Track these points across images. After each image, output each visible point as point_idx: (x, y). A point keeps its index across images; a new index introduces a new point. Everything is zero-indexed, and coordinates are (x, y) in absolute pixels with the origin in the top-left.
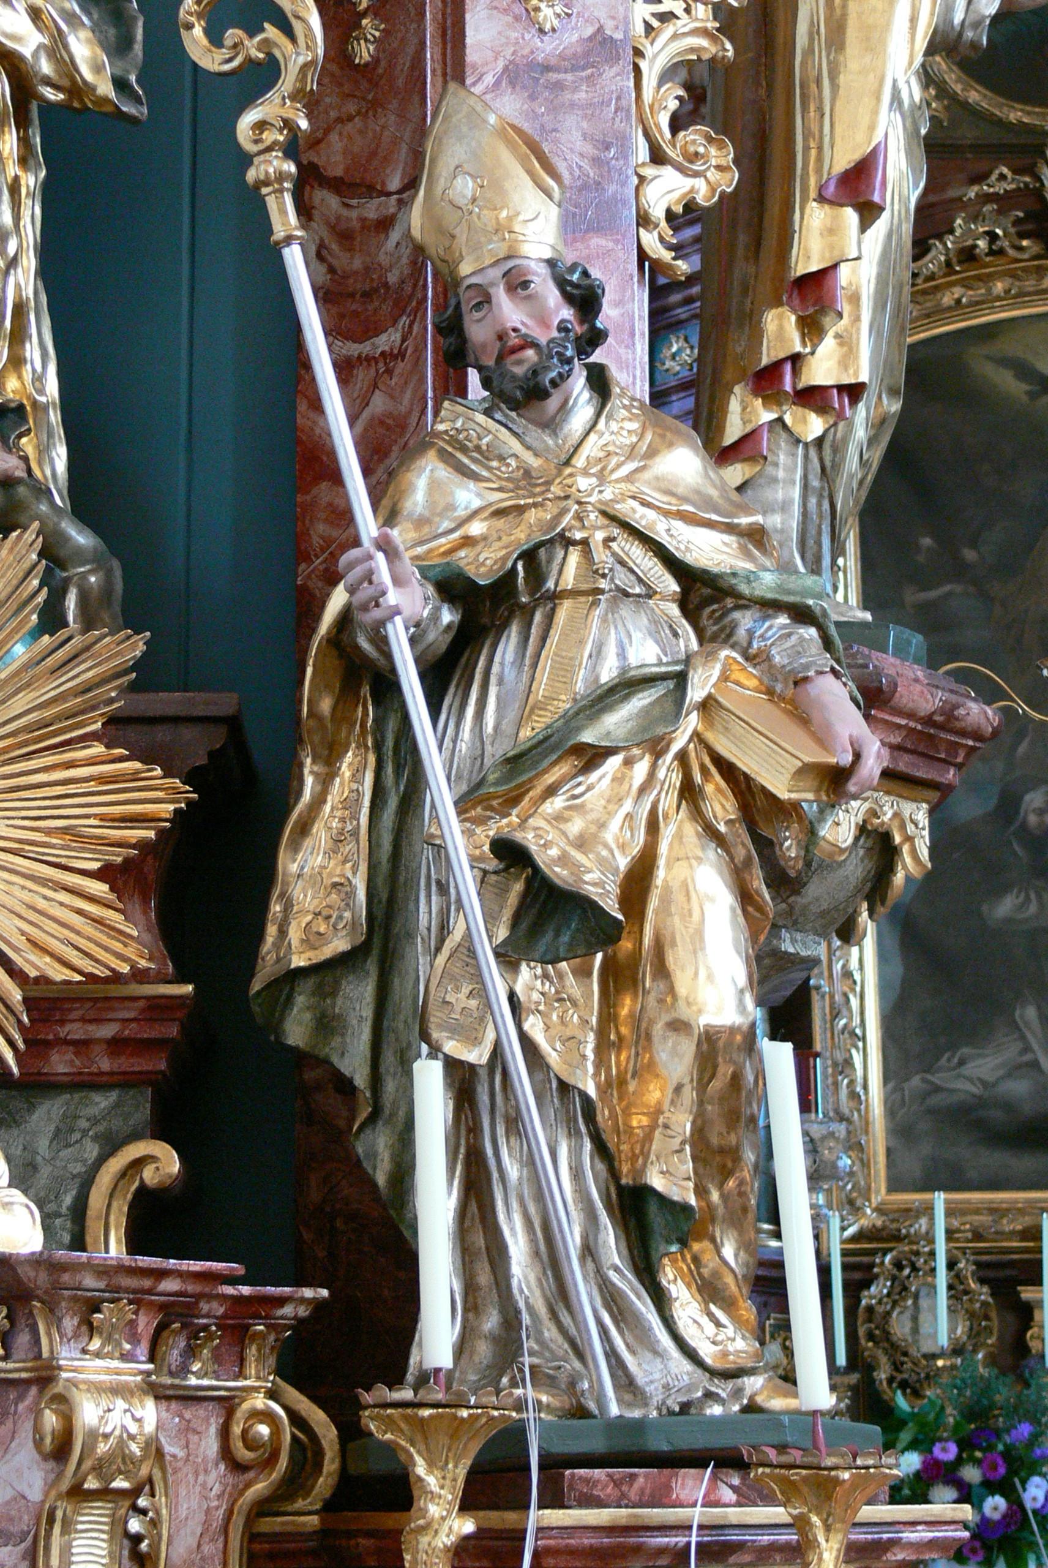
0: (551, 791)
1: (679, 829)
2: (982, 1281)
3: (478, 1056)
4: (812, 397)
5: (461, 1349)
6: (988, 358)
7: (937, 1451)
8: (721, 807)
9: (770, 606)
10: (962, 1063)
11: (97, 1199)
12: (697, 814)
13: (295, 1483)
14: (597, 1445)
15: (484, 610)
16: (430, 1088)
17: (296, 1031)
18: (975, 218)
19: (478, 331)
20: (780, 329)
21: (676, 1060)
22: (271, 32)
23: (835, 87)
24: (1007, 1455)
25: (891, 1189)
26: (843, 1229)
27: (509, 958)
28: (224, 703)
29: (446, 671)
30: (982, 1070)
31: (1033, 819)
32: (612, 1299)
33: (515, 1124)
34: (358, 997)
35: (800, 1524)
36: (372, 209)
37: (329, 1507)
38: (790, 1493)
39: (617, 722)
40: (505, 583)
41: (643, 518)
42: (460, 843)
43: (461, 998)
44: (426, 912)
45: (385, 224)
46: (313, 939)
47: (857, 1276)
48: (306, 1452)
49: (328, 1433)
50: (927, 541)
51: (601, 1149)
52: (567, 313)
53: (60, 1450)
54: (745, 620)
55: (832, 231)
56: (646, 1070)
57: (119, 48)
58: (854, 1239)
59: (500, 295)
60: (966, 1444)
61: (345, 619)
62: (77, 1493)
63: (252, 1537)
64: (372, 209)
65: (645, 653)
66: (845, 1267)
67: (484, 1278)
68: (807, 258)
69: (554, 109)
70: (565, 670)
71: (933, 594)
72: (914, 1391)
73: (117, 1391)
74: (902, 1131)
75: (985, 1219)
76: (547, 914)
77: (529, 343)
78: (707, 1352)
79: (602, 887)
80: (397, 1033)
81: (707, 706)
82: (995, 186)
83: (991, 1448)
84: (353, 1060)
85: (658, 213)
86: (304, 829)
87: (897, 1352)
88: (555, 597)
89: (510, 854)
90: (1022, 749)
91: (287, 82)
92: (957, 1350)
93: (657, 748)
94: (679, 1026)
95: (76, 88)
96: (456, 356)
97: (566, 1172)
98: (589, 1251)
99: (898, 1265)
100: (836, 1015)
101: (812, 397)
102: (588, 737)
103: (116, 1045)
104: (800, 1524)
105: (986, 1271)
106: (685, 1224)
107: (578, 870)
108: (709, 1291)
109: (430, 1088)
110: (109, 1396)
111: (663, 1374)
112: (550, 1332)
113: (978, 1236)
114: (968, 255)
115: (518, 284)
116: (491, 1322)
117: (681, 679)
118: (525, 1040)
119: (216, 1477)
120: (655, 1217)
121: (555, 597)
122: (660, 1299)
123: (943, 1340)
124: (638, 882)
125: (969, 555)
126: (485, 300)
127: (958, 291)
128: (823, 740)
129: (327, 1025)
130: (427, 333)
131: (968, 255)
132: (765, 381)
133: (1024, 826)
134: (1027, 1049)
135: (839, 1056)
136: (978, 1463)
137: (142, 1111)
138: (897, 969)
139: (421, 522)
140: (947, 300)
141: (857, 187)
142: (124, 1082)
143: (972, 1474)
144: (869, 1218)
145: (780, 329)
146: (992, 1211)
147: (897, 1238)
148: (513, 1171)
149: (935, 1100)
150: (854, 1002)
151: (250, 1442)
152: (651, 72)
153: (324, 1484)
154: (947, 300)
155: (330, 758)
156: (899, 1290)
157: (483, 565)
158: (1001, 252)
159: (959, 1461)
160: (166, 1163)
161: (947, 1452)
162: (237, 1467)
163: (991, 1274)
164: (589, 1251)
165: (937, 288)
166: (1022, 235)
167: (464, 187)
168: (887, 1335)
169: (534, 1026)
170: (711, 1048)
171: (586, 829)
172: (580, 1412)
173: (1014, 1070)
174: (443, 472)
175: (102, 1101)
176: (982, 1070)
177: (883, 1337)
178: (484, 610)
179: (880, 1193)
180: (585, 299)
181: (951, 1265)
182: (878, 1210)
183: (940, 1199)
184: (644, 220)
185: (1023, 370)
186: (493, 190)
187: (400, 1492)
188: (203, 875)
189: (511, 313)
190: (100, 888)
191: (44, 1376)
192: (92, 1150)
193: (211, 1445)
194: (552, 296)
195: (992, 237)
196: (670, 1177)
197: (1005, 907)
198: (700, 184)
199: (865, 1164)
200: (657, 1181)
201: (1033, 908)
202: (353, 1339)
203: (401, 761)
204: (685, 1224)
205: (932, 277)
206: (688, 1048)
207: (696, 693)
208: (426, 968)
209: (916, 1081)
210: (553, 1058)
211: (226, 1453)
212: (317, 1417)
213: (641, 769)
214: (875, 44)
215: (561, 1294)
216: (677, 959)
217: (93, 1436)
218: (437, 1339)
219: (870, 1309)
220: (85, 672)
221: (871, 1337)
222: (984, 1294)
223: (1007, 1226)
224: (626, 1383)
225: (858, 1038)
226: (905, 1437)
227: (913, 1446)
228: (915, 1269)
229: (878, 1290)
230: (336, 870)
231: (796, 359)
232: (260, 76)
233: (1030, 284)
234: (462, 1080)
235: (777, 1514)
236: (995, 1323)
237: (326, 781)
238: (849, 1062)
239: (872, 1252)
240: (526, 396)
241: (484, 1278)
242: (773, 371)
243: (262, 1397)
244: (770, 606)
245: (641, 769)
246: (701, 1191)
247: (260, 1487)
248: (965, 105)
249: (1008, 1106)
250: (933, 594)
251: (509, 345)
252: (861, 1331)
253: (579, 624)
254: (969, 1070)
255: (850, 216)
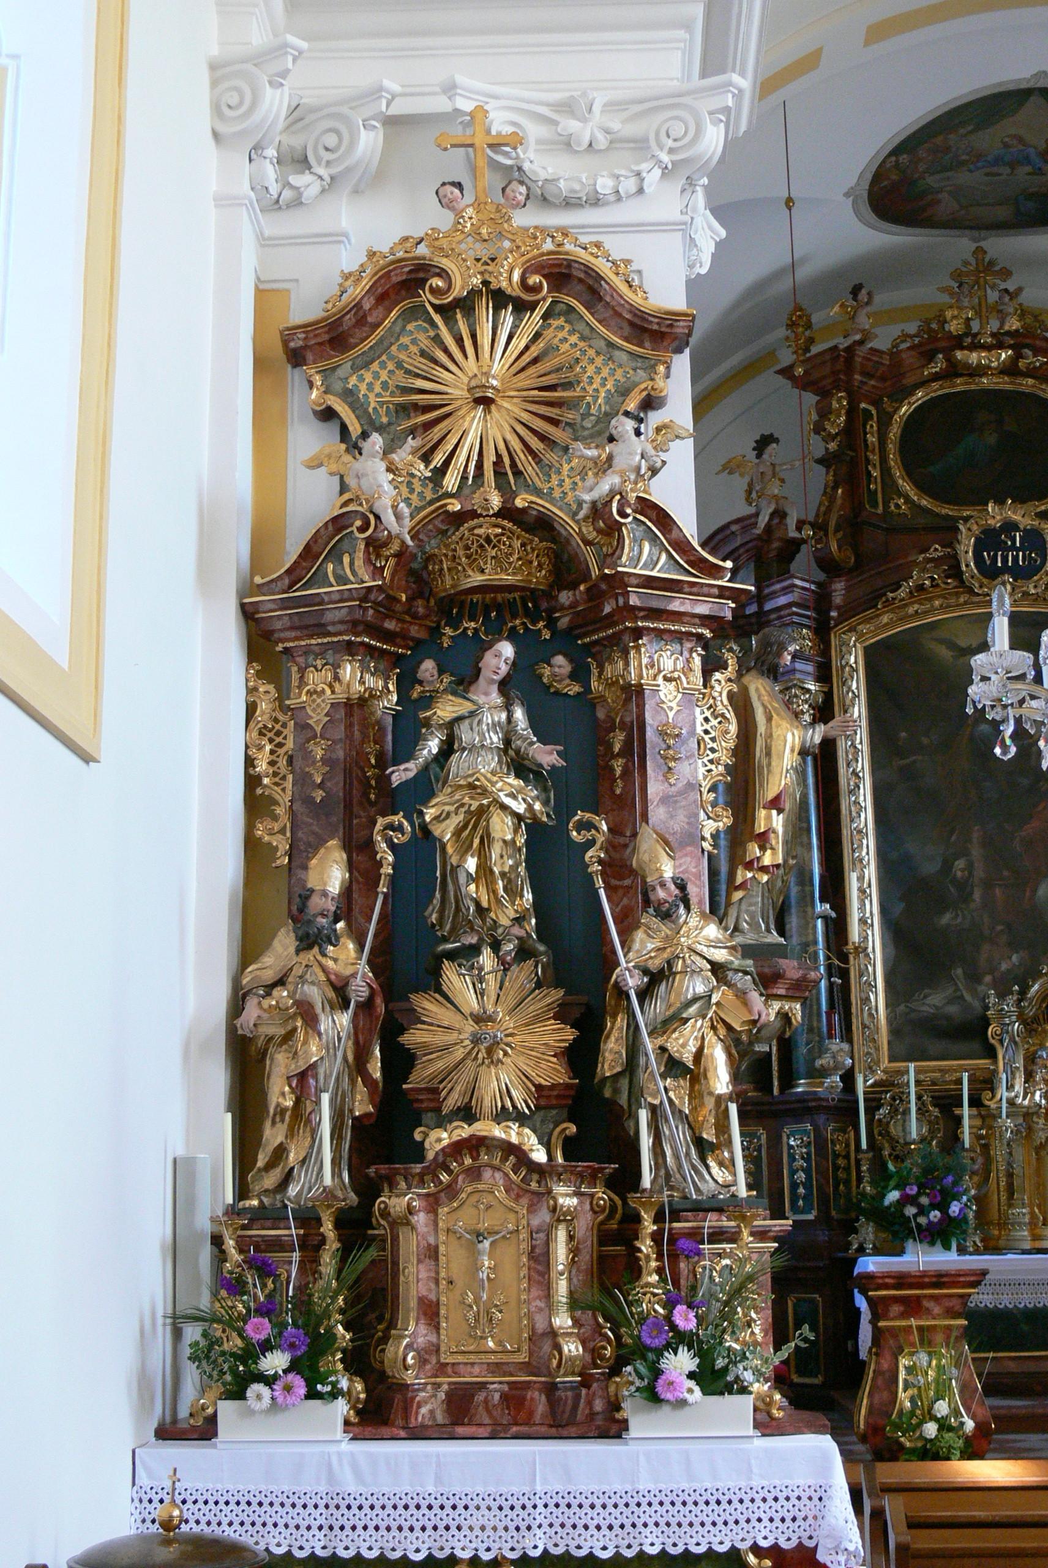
0: (674, 1031)
1: (710, 1037)
2: (935, 1106)
3: (656, 1102)
4: (764, 869)
5: (653, 1182)
6: (936, 640)
7: (908, 1190)
8: (722, 1032)
9: (737, 971)
10: (925, 997)
11: (553, 1140)
12: (716, 1034)
13: (611, 1216)
14: (688, 1206)
15: (656, 978)
16: (643, 1115)
17: (607, 1093)
18: (924, 570)
19: (652, 897)
20: (754, 850)
21: (710, 1103)
22: (593, 832)
23: (769, 771)
24: (941, 1191)
25: (890, 1061)
26: (865, 1081)
27: (664, 1076)
28: (584, 999)
29: (644, 994)
30: (934, 1001)
31: (959, 874)
32: (694, 1167)
33: (667, 1120)
34: (624, 1083)
35: (738, 1226)
36: (622, 840)
37: (621, 1222)
38: (735, 1219)
39: (693, 1010)
40: (662, 970)
41: (699, 948)
42: (649, 1045)
43: (652, 1086)
44: (642, 1061)
45: (626, 846)
46: (611, 1068)
47: (874, 1104)
48: (613, 1208)
49: (619, 1202)
50: (903, 734)
51: (690, 1126)
52: (677, 892)
53: (554, 1210)
54: (730, 974)
55: (769, 818)
56: (702, 1105)
57: (546, 803)
58: (872, 1086)
59: (658, 888)
60: (921, 1186)
61: (616, 982)
62: (559, 1221)
63: (599, 1231)
64: (622, 840)
65: (700, 989)
66: (865, 1100)
67: (660, 1161)
68: (761, 827)
69: (675, 809)
70: (679, 994)
71: (907, 761)
72: (898, 1159)
73: (567, 1195)
74: (895, 1032)
75: (938, 1075)
76: (673, 1066)
77: (666, 902)
78: (720, 1180)
79: (688, 1058)
80: (636, 1095)
81: (718, 1004)
82: (931, 554)
83: (933, 1189)
84: (623, 1100)
85: (708, 836)
86: (608, 1037)
87: (893, 1142)
88: (676, 973)
89: (663, 1049)
90: (953, 838)
91: (598, 845)
92: (923, 1140)
93: (704, 1017)
94: (711, 1094)
95: (534, 817)
96: (647, 902)
97: (678, 1135)
98: (688, 1154)
99: (893, 1099)
100: (861, 975)
101: (764, 869)
102: (684, 1015)
103: (558, 1097)
104: (738, 1226)
105: (937, 1101)
106: (713, 1147)
107: (681, 1054)
108: (721, 1164)
109: (643, 1115)
110: (566, 1198)
111: (708, 1187)
112: (678, 1176)
113: (934, 1083)
114: (921, 588)
115: (663, 885)
116: (662, 1172)
117: (710, 996)
118: (670, 1100)
119: (589, 1215)
120: (706, 1146)
121: (676, 973)
122: (707, 1167)
123: (914, 1135)
124: (699, 1055)
125: (925, 741)
126: (654, 889)
127: (916, 606)
128: (750, 1012)
129: (616, 1091)
130: (639, 900)
131: (921, 588)
132: (749, 866)
133: (955, 877)
134: (958, 989)
135: (864, 996)
136: (928, 1195)
137: (565, 1115)
138: (892, 951)
139: (638, 951)
140: (911, 610)
141: (775, 803)
142: (562, 1107)
143: (924, 1200)
144: (880, 1075)
145: (754, 850)
146: (941, 1071)
147: (893, 1085)
148: (667, 1133)
149: (913, 1015)
150: (870, 969)
151: (598, 1205)
152: (705, 790)
153: (618, 1216)
154: (911, 610)
155: (614, 1017)
156: (894, 1111)
157: (654, 965)
158: (937, 585)
159: (919, 1194)
160: (573, 1129)
161: (913, 1190)
162: (595, 1212)
163: (942, 1102)
164: (688, 1154)
165: (906, 605)
166: (948, 577)
167: (646, 857)
168: (888, 1133)
169: (671, 1094)
170: (719, 1099)
171: (683, 1044)
172: (685, 1198)
173: (951, 1001)
174: (644, 936)
175: (554, 1112)
176: (934, 1001)
177: (886, 1134)
178: (656, 978)
179: (885, 1063)
180: (682, 887)
181: (919, 1098)
182: (884, 1071)
183: (912, 1066)
184: (703, 839)
185: (951, 645)
186: (655, 859)
187: (638, 1219)
188: (581, 1055)
189: (661, 894)
190: (554, 1060)
191: (549, 1192)
192: (551, 1126)
193: (587, 1207)
194: (673, 887)
195: (933, 579)
196: (709, 1135)
197: (946, 919)
198: (721, 824)
199: (877, 1049)
200: (705, 1136)
201: (959, 920)
202: (625, 1179)
203: (632, 1016)
204: (713, 1147)
205: (903, 600)
206: (713, 1100)
207: (714, 1000)
208: (642, 1077)
209: (902, 1007)
210: (677, 1102)
211: (592, 1209)
212: (616, 1198)
213: (699, 1023)
214: (781, 757)
215: (680, 1167)
216: (710, 1075)
217: (562, 1206)
218: (646, 1181)
219: (880, 1120)
220: (549, 1000)
221: (880, 1134)
222: (936, 1112)
223: (948, 1077)
224: (698, 1190)
225: (872, 986)
226: (892, 1183)
227: (895, 1188)
228: (901, 1100)
229: (883, 1111)
230: (616, 1048)
231: (758, 859)
232: (591, 843)
233: (953, 601)
234: (654, 1110)
235: (733, 1224)
236: (941, 1126)
237: (613, 1024)
238: (868, 999)
239: (881, 1092)
240: (666, 915)
241: (660, 1161)
242: (751, 862)
243: (601, 1194)
244: (737, 971)
245: (699, 1023)
246: (717, 1138)
247: (601, 1217)
248: (919, 506)
249: (948, 1018)
250: (907, 761)
251: (660, 903)
252: (876, 1132)
253: (682, 981)
254: (929, 1001)
255: (774, 812)
